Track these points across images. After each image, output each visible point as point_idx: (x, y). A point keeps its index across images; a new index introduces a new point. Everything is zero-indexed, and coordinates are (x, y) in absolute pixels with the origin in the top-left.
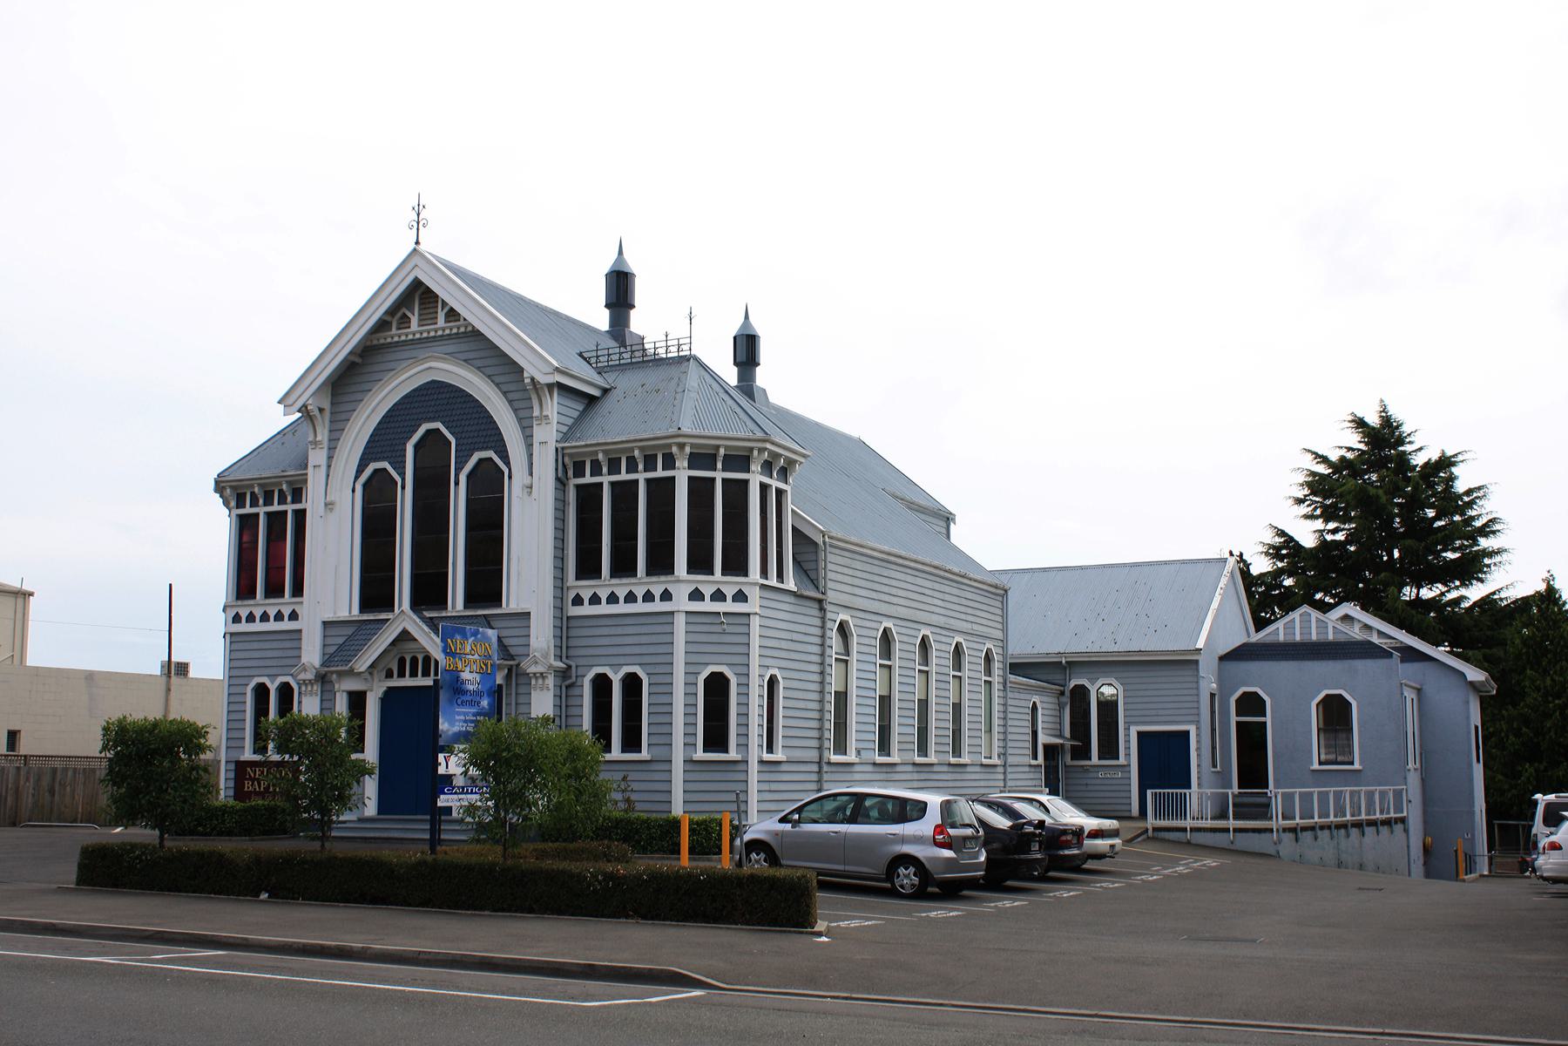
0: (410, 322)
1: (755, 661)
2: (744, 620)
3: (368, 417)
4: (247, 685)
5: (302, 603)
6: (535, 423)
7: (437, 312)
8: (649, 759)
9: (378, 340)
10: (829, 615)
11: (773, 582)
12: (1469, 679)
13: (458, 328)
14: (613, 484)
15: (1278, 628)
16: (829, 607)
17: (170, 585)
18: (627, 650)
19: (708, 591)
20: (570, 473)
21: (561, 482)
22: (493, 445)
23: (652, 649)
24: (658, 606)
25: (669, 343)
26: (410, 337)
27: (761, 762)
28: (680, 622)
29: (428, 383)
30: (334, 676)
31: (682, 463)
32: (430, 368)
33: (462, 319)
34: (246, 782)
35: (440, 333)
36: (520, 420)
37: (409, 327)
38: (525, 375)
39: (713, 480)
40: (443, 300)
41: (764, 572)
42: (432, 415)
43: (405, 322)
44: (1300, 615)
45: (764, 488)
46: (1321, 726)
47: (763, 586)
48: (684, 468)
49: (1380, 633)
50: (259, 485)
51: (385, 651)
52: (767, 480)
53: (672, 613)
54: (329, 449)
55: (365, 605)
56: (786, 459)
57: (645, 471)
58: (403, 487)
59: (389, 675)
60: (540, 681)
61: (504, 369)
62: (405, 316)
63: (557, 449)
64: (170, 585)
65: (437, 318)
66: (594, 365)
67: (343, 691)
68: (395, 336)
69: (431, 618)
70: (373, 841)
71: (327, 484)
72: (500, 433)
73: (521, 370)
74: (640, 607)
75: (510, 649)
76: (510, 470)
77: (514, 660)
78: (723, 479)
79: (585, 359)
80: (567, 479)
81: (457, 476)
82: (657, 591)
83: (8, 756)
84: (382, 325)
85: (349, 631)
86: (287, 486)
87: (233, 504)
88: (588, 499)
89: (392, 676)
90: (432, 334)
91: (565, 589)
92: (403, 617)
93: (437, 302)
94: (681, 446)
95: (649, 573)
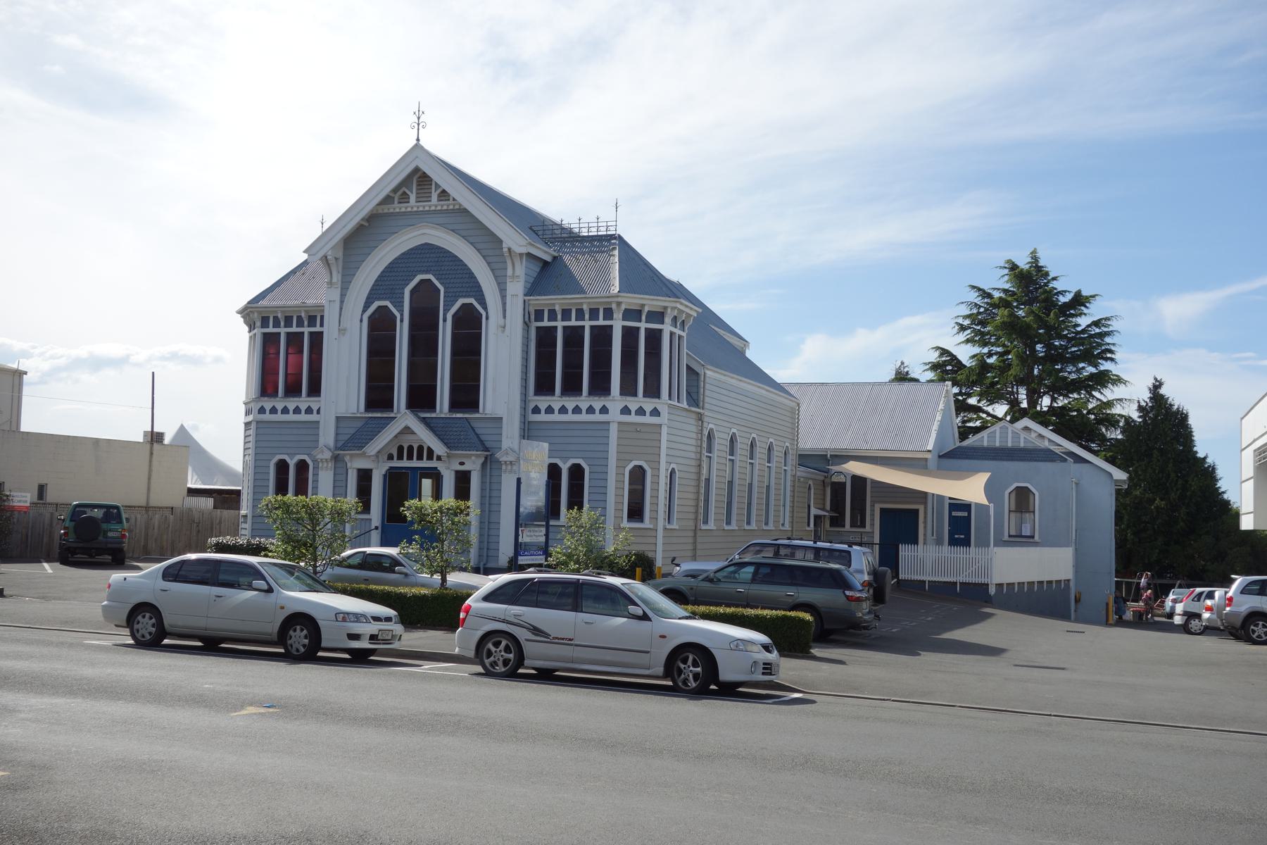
1: (663, 459)
3: (374, 267)
4: (271, 460)
9: (389, 209)
10: (705, 425)
11: (676, 403)
12: (1115, 478)
13: (448, 206)
14: (565, 328)
16: (706, 419)
17: (153, 373)
19: (633, 408)
20: (533, 317)
21: (526, 325)
24: (597, 417)
26: (409, 209)
27: (665, 529)
28: (614, 429)
31: (618, 315)
33: (451, 199)
35: (433, 208)
36: (496, 277)
37: (408, 202)
38: (504, 245)
40: (436, 183)
42: (425, 269)
43: (405, 198)
45: (672, 334)
46: (1013, 508)
47: (670, 406)
49: (1050, 440)
50: (282, 312)
51: (391, 440)
53: (609, 423)
54: (342, 289)
55: (371, 404)
58: (402, 321)
59: (390, 457)
60: (509, 467)
61: (489, 244)
62: (405, 193)
63: (524, 301)
64: (153, 373)
65: (431, 197)
66: (541, 237)
68: (397, 207)
69: (424, 418)
71: (340, 315)
73: (501, 241)
76: (487, 313)
77: (489, 451)
79: (534, 231)
84: (387, 200)
85: (359, 424)
88: (545, 338)
89: (392, 459)
90: (427, 208)
91: (527, 401)
92: (403, 418)
93: (431, 185)
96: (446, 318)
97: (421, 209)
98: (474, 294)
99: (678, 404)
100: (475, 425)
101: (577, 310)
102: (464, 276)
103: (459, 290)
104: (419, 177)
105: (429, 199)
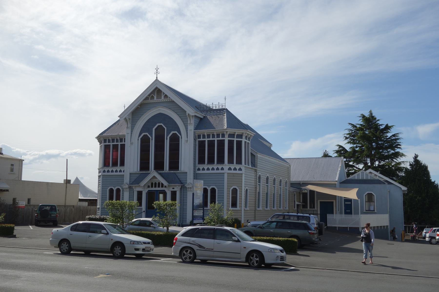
0: (154, 98)
4: (107, 188)
5: (124, 168)
6: (188, 125)
7: (161, 96)
12: (403, 189)
14: (208, 141)
15: (355, 176)
16: (258, 171)
17: (67, 159)
20: (197, 137)
21: (195, 140)
22: (177, 130)
24: (118, 173)
26: (154, 101)
27: (244, 210)
28: (226, 175)
29: (159, 113)
30: (134, 187)
31: (226, 136)
33: (168, 98)
35: (162, 101)
37: (161, 98)
38: (187, 113)
39: (233, 140)
40: (163, 92)
43: (152, 98)
44: (361, 173)
45: (245, 142)
46: (367, 200)
47: (245, 167)
48: (227, 137)
53: (224, 173)
55: (142, 168)
56: (250, 135)
57: (217, 138)
58: (152, 139)
59: (149, 187)
60: (190, 189)
61: (181, 112)
62: (152, 96)
63: (194, 132)
64: (67, 159)
67: (136, 191)
68: (150, 101)
69: (160, 173)
71: (131, 138)
72: (179, 127)
73: (185, 112)
74: (215, 171)
75: (181, 181)
77: (182, 184)
78: (236, 140)
80: (196, 139)
81: (167, 137)
83: (28, 205)
84: (147, 98)
88: (202, 144)
90: (160, 101)
92: (153, 173)
93: (161, 93)
97: (158, 101)
99: (248, 166)
100: (178, 175)
104: (157, 91)
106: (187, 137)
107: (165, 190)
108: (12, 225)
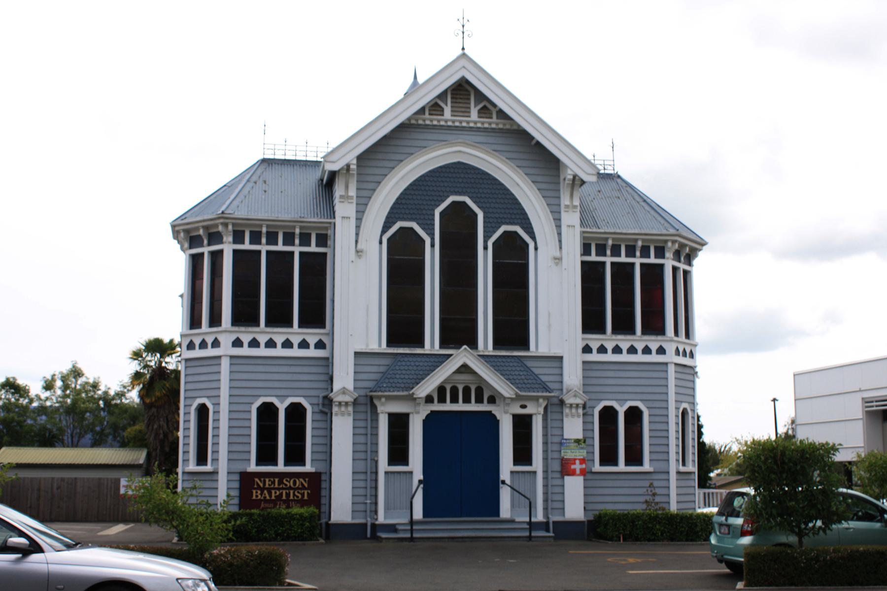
2: (663, 368)
4: (252, 403)
8: (211, 471)
9: (424, 120)
14: (613, 264)
18: (630, 389)
23: (650, 389)
24: (654, 358)
25: (308, 149)
26: (442, 123)
27: (678, 473)
28: (225, 364)
32: (460, 152)
34: (254, 491)
35: (472, 125)
37: (469, 116)
41: (676, 333)
45: (675, 269)
48: (230, 243)
52: (677, 264)
58: (433, 245)
68: (428, 119)
70: (460, 540)
72: (526, 214)
76: (536, 243)
82: (654, 347)
86: (203, 231)
87: (186, 245)
90: (464, 124)
94: (226, 225)
95: (267, 325)
96: (487, 246)
97: (457, 124)
98: (519, 221)
99: (687, 341)
100: (529, 364)
101: (317, 235)
102: (506, 201)
103: (501, 216)
105: (467, 113)
106: (561, 248)
107: (493, 412)
108: (718, 544)
